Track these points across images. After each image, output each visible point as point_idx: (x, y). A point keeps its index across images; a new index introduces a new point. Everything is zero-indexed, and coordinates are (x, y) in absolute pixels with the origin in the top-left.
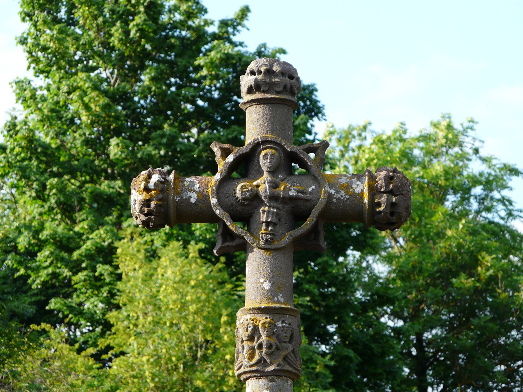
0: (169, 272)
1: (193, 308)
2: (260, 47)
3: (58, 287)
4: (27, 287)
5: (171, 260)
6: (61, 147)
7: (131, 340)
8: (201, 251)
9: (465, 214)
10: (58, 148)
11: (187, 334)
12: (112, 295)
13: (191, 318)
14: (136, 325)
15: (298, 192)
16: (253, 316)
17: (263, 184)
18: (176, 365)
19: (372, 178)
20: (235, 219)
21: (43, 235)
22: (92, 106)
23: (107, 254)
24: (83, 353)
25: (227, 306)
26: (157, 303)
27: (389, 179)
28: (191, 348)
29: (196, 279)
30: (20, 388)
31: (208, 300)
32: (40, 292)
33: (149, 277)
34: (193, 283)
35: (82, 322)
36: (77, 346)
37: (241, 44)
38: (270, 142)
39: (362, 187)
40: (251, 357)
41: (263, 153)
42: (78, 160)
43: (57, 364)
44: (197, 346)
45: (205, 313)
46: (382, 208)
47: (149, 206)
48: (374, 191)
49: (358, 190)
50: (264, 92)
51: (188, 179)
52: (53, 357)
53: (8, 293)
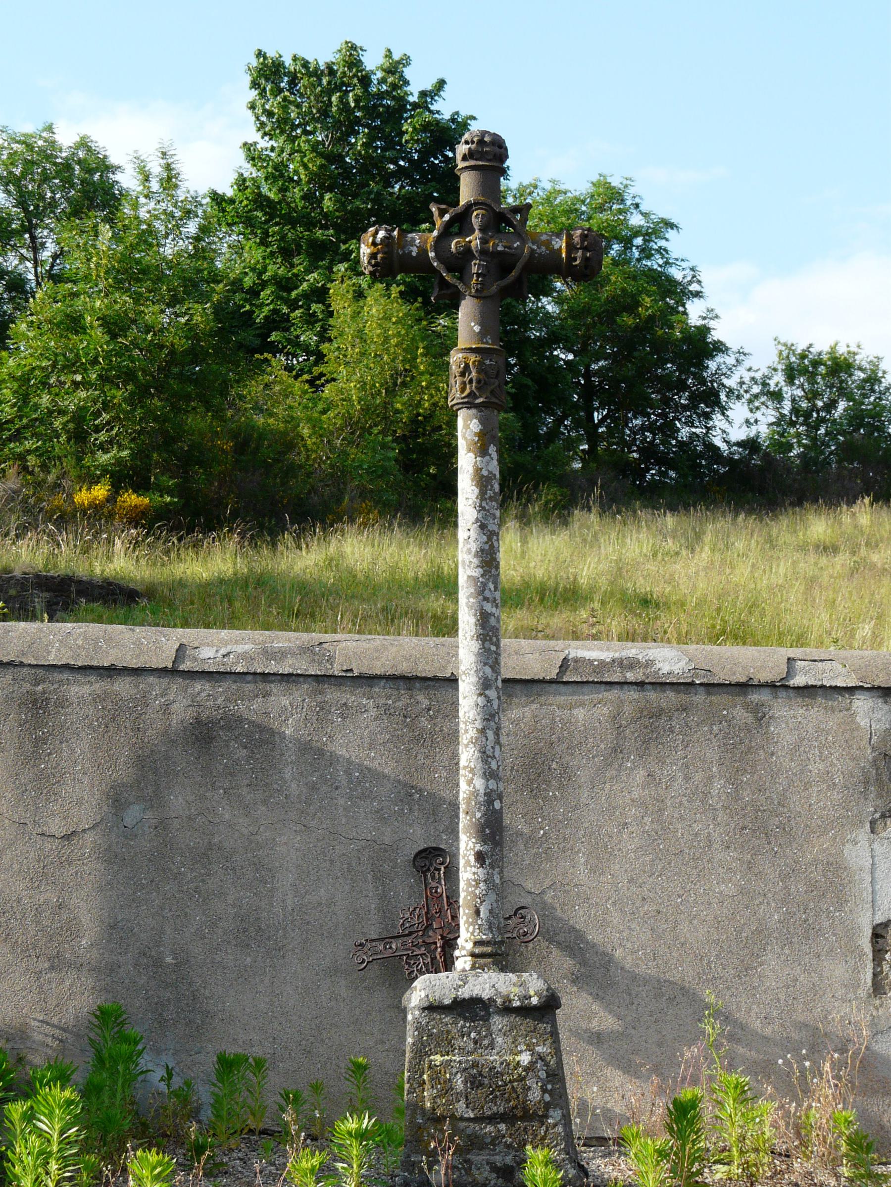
0: (374, 310)
1: (394, 341)
2: (453, 115)
3: (277, 321)
4: (252, 321)
5: (376, 300)
6: (283, 200)
7: (341, 368)
8: (401, 292)
9: (627, 262)
10: (280, 203)
11: (388, 364)
12: (324, 329)
13: (392, 350)
14: (345, 356)
15: (505, 247)
16: (465, 355)
17: (475, 240)
18: (379, 391)
19: (570, 237)
20: (449, 270)
21: (265, 277)
22: (310, 165)
23: (320, 294)
24: (300, 379)
25: (423, 340)
26: (363, 336)
27: (584, 237)
28: (392, 376)
29: (397, 316)
30: (246, 409)
31: (407, 334)
32: (263, 326)
33: (357, 314)
34: (394, 320)
35: (298, 351)
36: (294, 373)
37: (438, 112)
38: (482, 204)
39: (561, 244)
40: (463, 390)
41: (475, 213)
42: (296, 212)
43: (277, 388)
44: (397, 374)
45: (404, 346)
46: (578, 262)
47: (376, 258)
48: (571, 247)
49: (556, 247)
50: (476, 160)
51: (410, 235)
52: (274, 382)
53: (235, 327)
